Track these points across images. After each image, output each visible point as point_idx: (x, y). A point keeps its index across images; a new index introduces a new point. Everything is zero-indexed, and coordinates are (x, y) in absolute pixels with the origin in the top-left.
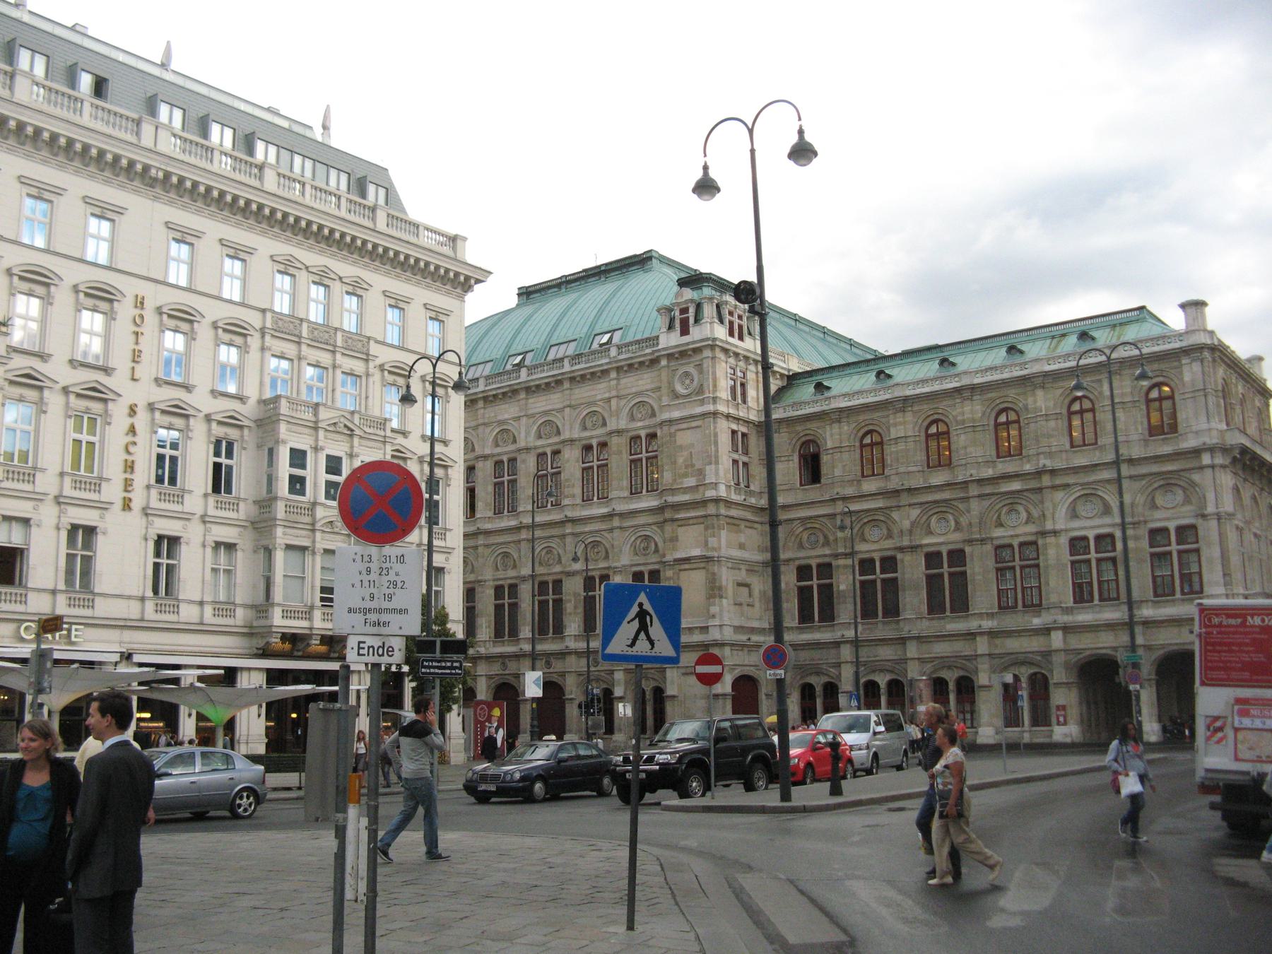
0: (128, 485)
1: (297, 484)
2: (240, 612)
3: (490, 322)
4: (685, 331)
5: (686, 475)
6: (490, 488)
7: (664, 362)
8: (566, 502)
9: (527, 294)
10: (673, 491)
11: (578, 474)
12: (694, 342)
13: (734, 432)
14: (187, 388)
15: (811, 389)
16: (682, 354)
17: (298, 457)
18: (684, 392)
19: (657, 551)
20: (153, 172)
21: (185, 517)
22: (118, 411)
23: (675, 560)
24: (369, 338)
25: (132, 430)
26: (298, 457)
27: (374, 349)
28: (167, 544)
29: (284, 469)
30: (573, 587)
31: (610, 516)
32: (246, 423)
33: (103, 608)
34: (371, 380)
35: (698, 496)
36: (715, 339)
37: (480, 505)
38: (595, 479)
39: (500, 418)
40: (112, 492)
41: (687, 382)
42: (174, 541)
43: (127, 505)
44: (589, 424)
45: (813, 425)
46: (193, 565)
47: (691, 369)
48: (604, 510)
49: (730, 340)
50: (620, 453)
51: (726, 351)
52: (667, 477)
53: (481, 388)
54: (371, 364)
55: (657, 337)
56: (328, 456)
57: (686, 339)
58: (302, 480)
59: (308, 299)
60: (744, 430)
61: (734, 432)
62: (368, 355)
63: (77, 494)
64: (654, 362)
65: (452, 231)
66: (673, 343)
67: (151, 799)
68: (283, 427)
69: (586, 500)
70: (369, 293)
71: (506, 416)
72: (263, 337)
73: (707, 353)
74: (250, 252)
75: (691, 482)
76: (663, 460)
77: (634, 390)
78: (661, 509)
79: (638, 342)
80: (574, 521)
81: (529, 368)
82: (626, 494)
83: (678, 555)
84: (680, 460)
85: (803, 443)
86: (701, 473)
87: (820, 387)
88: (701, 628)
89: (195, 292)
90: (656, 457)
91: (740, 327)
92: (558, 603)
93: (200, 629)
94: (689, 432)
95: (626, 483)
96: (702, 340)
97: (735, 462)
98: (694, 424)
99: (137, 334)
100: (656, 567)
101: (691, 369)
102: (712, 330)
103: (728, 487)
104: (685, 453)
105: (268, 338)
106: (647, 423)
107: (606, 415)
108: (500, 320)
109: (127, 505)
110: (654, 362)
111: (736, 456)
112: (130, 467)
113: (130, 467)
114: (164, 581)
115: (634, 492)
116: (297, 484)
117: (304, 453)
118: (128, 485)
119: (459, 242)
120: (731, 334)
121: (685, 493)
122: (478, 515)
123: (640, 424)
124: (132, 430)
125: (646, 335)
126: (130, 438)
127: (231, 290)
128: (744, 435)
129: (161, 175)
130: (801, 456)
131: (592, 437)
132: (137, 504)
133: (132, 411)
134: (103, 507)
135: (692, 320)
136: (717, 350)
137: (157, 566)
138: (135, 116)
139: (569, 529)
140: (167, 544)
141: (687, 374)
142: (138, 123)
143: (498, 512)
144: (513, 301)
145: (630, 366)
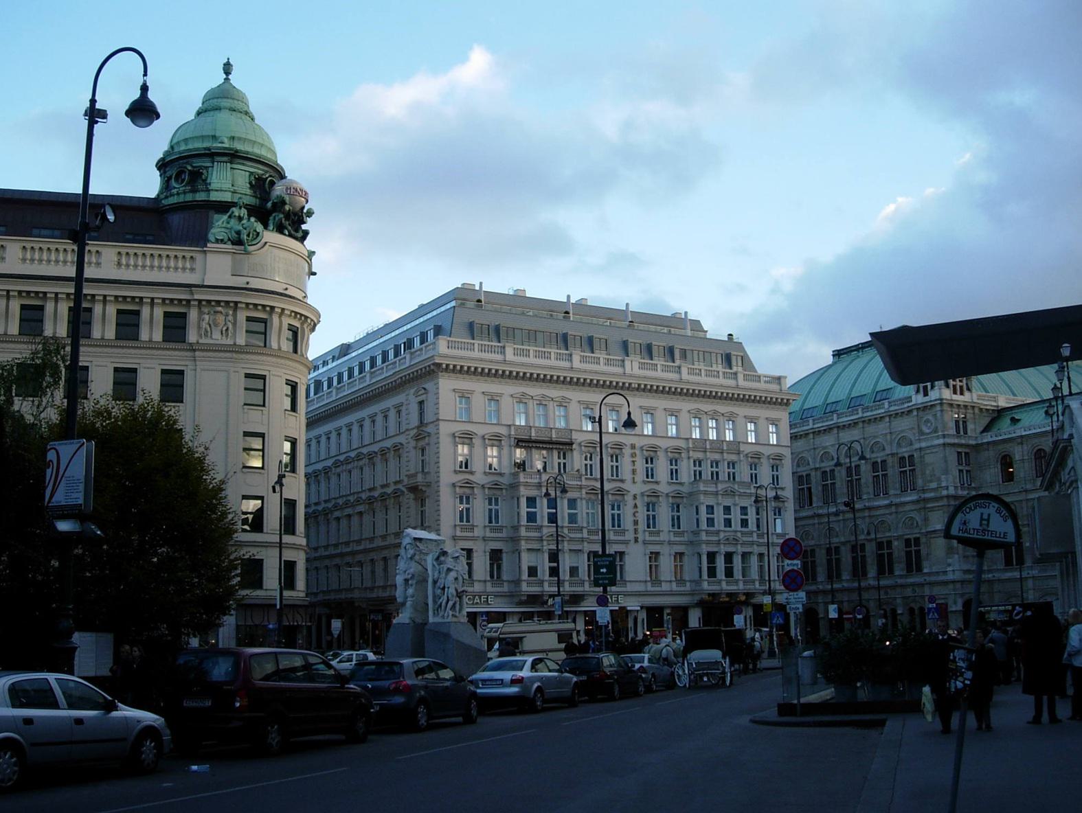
0: (636, 531)
1: (711, 522)
2: (688, 584)
3: (818, 375)
4: (926, 394)
5: (931, 481)
6: (820, 488)
7: (915, 413)
8: (865, 497)
9: (838, 354)
10: (924, 491)
11: (871, 480)
12: (931, 401)
13: (959, 453)
14: (657, 483)
15: (1009, 421)
16: (925, 408)
17: (710, 509)
18: (928, 431)
19: (917, 526)
20: (633, 385)
21: (661, 543)
22: (629, 498)
23: (927, 532)
24: (739, 443)
25: (636, 506)
26: (710, 509)
27: (742, 448)
28: (655, 556)
29: (704, 515)
30: (870, 548)
31: (890, 505)
32: (684, 495)
33: (630, 588)
34: (742, 463)
35: (938, 495)
36: (941, 399)
37: (814, 499)
38: (880, 485)
39: (823, 445)
40: (630, 536)
41: (929, 425)
42: (657, 554)
43: (636, 540)
44: (875, 450)
45: (1007, 446)
46: (666, 565)
47: (930, 417)
48: (886, 502)
49: (955, 397)
50: (893, 467)
51: (951, 405)
52: (920, 482)
53: (811, 426)
54: (742, 456)
55: (911, 397)
56: (724, 507)
57: (927, 399)
58: (713, 519)
59: (708, 428)
60: (967, 450)
61: (959, 453)
62: (739, 451)
63: (616, 538)
64: (910, 412)
65: (777, 374)
66: (919, 402)
67: (1065, 646)
68: (702, 497)
69: (877, 495)
70: (738, 419)
71: (827, 444)
72: (689, 452)
73: (938, 408)
74: (679, 411)
75: (934, 485)
76: (918, 472)
77: (900, 429)
78: (917, 502)
79: (900, 400)
80: (869, 509)
81: (838, 415)
82: (899, 492)
83: (929, 529)
84: (928, 472)
85: (1002, 459)
86: (939, 480)
87: (1014, 421)
88: (944, 572)
89: (657, 437)
90: (914, 469)
91: (961, 387)
92: (864, 557)
93: (671, 594)
94: (931, 455)
95: (898, 486)
96: (936, 400)
97: (960, 471)
98: (934, 450)
99: (633, 462)
100: (918, 535)
101: (930, 417)
102: (940, 394)
103: (956, 487)
104: (930, 468)
105: (691, 452)
106: (908, 449)
107: (885, 444)
108: (825, 371)
109: (636, 540)
110: (910, 412)
111: (961, 468)
112: (636, 523)
113: (636, 523)
114: (654, 569)
115: (904, 490)
116: (711, 522)
117: (730, 507)
118: (636, 531)
119: (782, 380)
120: (955, 392)
121: (931, 492)
122: (814, 505)
123: (904, 450)
124: (636, 506)
125: (906, 395)
126: (635, 510)
127: (672, 431)
128: (966, 454)
129: (637, 386)
130: (1001, 464)
131: (877, 457)
132: (640, 540)
133: (635, 497)
134: (626, 542)
135: (929, 387)
136: (945, 405)
137: (651, 566)
138: (620, 358)
139: (866, 514)
140: (655, 556)
141: (928, 421)
142: (623, 361)
143: (826, 503)
144: (830, 360)
145: (897, 414)
